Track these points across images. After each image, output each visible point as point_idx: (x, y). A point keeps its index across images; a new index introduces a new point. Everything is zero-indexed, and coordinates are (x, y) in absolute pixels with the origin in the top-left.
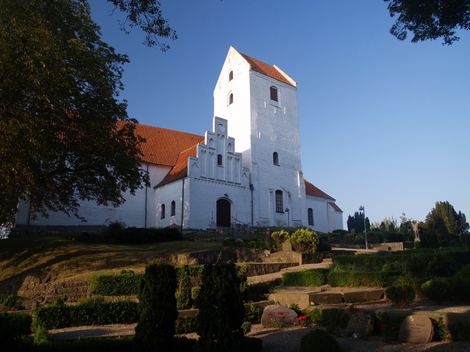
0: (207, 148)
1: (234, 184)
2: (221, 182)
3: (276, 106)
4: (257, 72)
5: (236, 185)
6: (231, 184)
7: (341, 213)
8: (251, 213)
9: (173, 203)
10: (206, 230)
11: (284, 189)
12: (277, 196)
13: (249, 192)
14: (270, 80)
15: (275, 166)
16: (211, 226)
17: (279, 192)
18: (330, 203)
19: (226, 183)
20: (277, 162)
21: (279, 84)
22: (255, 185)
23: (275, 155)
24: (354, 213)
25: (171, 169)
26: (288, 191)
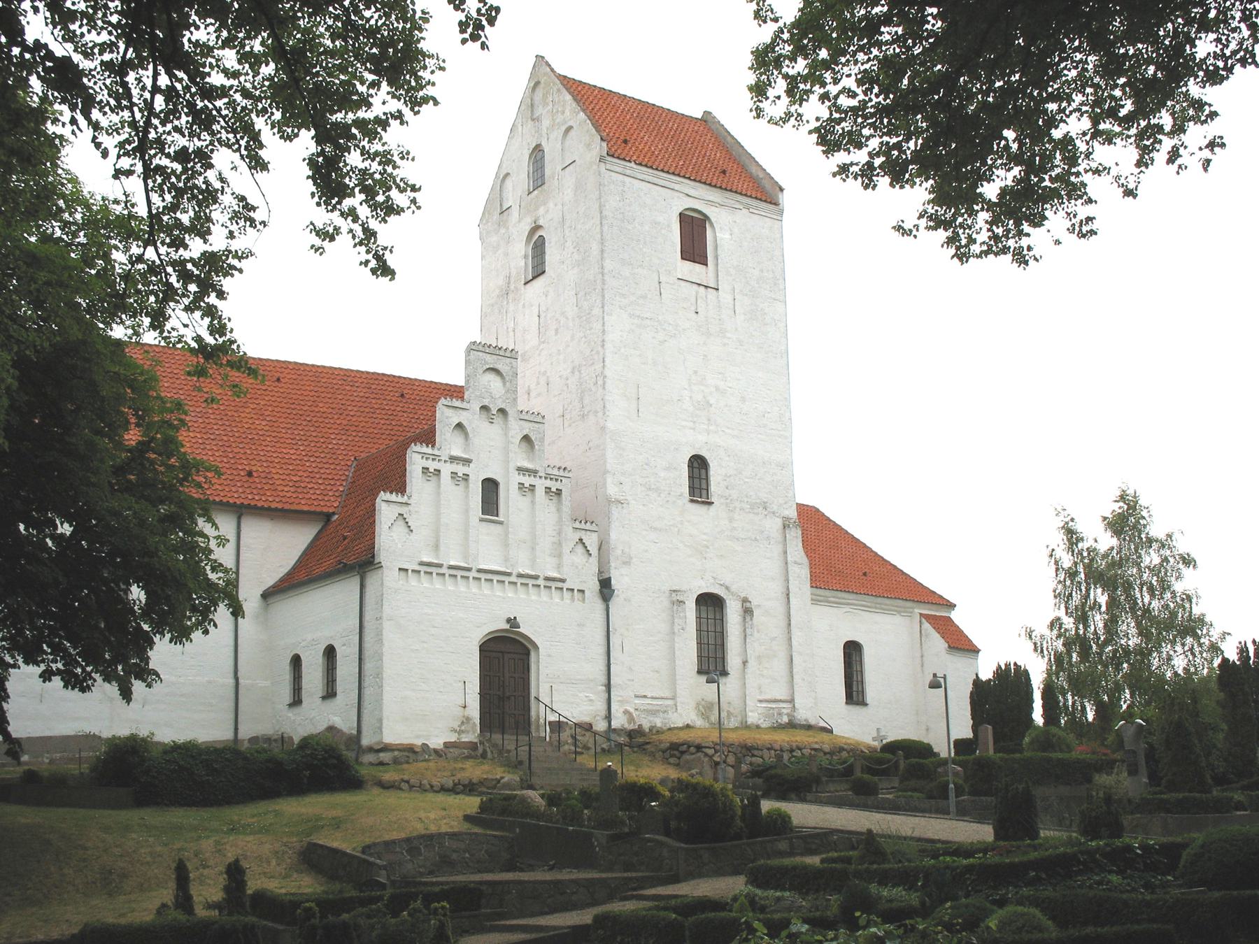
0: (443, 458)
1: (541, 582)
2: (496, 578)
3: (699, 284)
4: (630, 161)
5: (549, 584)
6: (531, 582)
7: (971, 655)
8: (603, 679)
9: (330, 652)
10: (442, 747)
11: (727, 588)
12: (704, 615)
13: (599, 605)
14: (677, 187)
15: (694, 506)
17: (710, 603)
18: (927, 617)
19: (513, 579)
20: (704, 492)
21: (711, 198)
22: (619, 582)
23: (698, 465)
24: (970, 688)
25: (322, 524)
26: (743, 595)
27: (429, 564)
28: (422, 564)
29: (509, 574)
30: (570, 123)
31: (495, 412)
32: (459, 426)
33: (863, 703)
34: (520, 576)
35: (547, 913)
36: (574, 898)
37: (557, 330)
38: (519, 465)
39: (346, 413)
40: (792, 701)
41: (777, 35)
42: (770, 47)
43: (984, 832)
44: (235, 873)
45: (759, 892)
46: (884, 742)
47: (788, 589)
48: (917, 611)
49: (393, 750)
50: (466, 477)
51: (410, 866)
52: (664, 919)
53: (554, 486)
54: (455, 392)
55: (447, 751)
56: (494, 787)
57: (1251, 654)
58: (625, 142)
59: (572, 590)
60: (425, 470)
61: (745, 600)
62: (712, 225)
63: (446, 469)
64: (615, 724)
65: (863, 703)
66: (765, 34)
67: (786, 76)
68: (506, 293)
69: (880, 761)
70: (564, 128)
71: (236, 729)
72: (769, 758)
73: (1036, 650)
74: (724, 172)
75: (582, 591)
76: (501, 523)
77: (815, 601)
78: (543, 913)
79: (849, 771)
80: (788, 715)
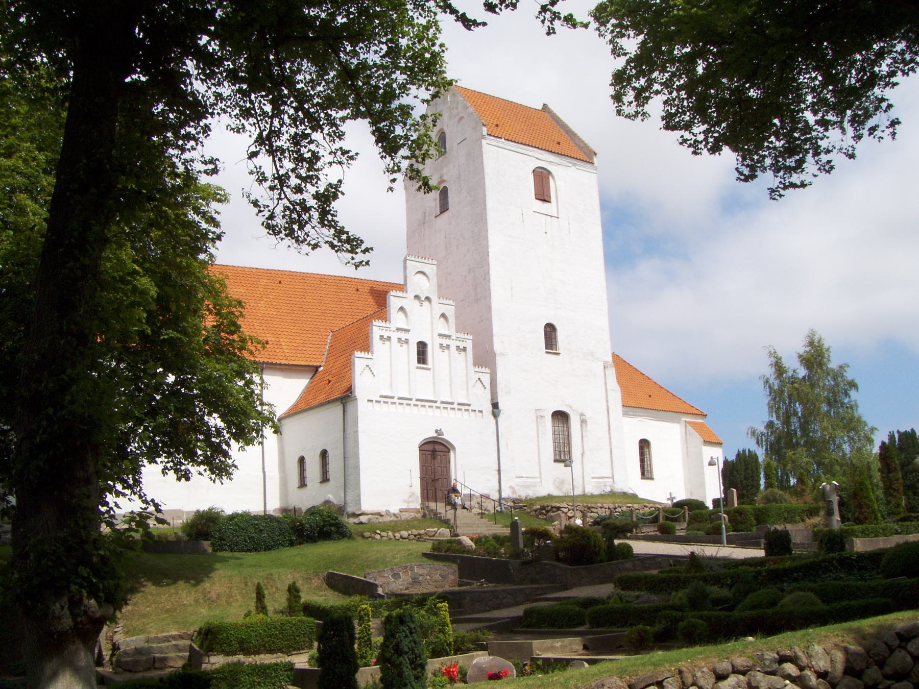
1: (455, 406)
2: (427, 404)
5: (460, 407)
6: (449, 406)
11: (570, 407)
14: (531, 153)
16: (409, 502)
17: (561, 417)
18: (691, 423)
19: (438, 404)
21: (552, 160)
23: (550, 331)
27: (385, 397)
28: (381, 396)
29: (436, 402)
30: (462, 115)
31: (423, 299)
32: (402, 309)
33: (652, 478)
34: (443, 402)
35: (488, 611)
36: (504, 601)
37: (458, 247)
38: (440, 332)
39: (323, 302)
40: (613, 478)
41: (628, 62)
42: (624, 70)
43: (760, 553)
44: (293, 591)
45: (623, 592)
46: (675, 501)
47: (608, 407)
48: (683, 419)
49: (368, 514)
50: (407, 341)
51: (394, 585)
52: (572, 610)
53: (462, 346)
54: (401, 288)
55: (401, 514)
56: (434, 536)
57: (897, 439)
58: (497, 126)
59: (475, 411)
60: (382, 337)
61: (582, 415)
62: (553, 178)
63: (395, 336)
64: (504, 495)
65: (652, 478)
66: (621, 63)
67: (634, 89)
68: (423, 223)
69: (673, 513)
70: (458, 118)
71: (265, 504)
72: (604, 513)
73: (758, 443)
74: (559, 143)
75: (481, 412)
76: (429, 369)
77: (625, 414)
78: (485, 611)
79: (655, 520)
80: (610, 486)
